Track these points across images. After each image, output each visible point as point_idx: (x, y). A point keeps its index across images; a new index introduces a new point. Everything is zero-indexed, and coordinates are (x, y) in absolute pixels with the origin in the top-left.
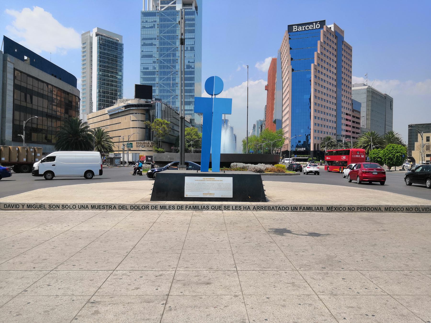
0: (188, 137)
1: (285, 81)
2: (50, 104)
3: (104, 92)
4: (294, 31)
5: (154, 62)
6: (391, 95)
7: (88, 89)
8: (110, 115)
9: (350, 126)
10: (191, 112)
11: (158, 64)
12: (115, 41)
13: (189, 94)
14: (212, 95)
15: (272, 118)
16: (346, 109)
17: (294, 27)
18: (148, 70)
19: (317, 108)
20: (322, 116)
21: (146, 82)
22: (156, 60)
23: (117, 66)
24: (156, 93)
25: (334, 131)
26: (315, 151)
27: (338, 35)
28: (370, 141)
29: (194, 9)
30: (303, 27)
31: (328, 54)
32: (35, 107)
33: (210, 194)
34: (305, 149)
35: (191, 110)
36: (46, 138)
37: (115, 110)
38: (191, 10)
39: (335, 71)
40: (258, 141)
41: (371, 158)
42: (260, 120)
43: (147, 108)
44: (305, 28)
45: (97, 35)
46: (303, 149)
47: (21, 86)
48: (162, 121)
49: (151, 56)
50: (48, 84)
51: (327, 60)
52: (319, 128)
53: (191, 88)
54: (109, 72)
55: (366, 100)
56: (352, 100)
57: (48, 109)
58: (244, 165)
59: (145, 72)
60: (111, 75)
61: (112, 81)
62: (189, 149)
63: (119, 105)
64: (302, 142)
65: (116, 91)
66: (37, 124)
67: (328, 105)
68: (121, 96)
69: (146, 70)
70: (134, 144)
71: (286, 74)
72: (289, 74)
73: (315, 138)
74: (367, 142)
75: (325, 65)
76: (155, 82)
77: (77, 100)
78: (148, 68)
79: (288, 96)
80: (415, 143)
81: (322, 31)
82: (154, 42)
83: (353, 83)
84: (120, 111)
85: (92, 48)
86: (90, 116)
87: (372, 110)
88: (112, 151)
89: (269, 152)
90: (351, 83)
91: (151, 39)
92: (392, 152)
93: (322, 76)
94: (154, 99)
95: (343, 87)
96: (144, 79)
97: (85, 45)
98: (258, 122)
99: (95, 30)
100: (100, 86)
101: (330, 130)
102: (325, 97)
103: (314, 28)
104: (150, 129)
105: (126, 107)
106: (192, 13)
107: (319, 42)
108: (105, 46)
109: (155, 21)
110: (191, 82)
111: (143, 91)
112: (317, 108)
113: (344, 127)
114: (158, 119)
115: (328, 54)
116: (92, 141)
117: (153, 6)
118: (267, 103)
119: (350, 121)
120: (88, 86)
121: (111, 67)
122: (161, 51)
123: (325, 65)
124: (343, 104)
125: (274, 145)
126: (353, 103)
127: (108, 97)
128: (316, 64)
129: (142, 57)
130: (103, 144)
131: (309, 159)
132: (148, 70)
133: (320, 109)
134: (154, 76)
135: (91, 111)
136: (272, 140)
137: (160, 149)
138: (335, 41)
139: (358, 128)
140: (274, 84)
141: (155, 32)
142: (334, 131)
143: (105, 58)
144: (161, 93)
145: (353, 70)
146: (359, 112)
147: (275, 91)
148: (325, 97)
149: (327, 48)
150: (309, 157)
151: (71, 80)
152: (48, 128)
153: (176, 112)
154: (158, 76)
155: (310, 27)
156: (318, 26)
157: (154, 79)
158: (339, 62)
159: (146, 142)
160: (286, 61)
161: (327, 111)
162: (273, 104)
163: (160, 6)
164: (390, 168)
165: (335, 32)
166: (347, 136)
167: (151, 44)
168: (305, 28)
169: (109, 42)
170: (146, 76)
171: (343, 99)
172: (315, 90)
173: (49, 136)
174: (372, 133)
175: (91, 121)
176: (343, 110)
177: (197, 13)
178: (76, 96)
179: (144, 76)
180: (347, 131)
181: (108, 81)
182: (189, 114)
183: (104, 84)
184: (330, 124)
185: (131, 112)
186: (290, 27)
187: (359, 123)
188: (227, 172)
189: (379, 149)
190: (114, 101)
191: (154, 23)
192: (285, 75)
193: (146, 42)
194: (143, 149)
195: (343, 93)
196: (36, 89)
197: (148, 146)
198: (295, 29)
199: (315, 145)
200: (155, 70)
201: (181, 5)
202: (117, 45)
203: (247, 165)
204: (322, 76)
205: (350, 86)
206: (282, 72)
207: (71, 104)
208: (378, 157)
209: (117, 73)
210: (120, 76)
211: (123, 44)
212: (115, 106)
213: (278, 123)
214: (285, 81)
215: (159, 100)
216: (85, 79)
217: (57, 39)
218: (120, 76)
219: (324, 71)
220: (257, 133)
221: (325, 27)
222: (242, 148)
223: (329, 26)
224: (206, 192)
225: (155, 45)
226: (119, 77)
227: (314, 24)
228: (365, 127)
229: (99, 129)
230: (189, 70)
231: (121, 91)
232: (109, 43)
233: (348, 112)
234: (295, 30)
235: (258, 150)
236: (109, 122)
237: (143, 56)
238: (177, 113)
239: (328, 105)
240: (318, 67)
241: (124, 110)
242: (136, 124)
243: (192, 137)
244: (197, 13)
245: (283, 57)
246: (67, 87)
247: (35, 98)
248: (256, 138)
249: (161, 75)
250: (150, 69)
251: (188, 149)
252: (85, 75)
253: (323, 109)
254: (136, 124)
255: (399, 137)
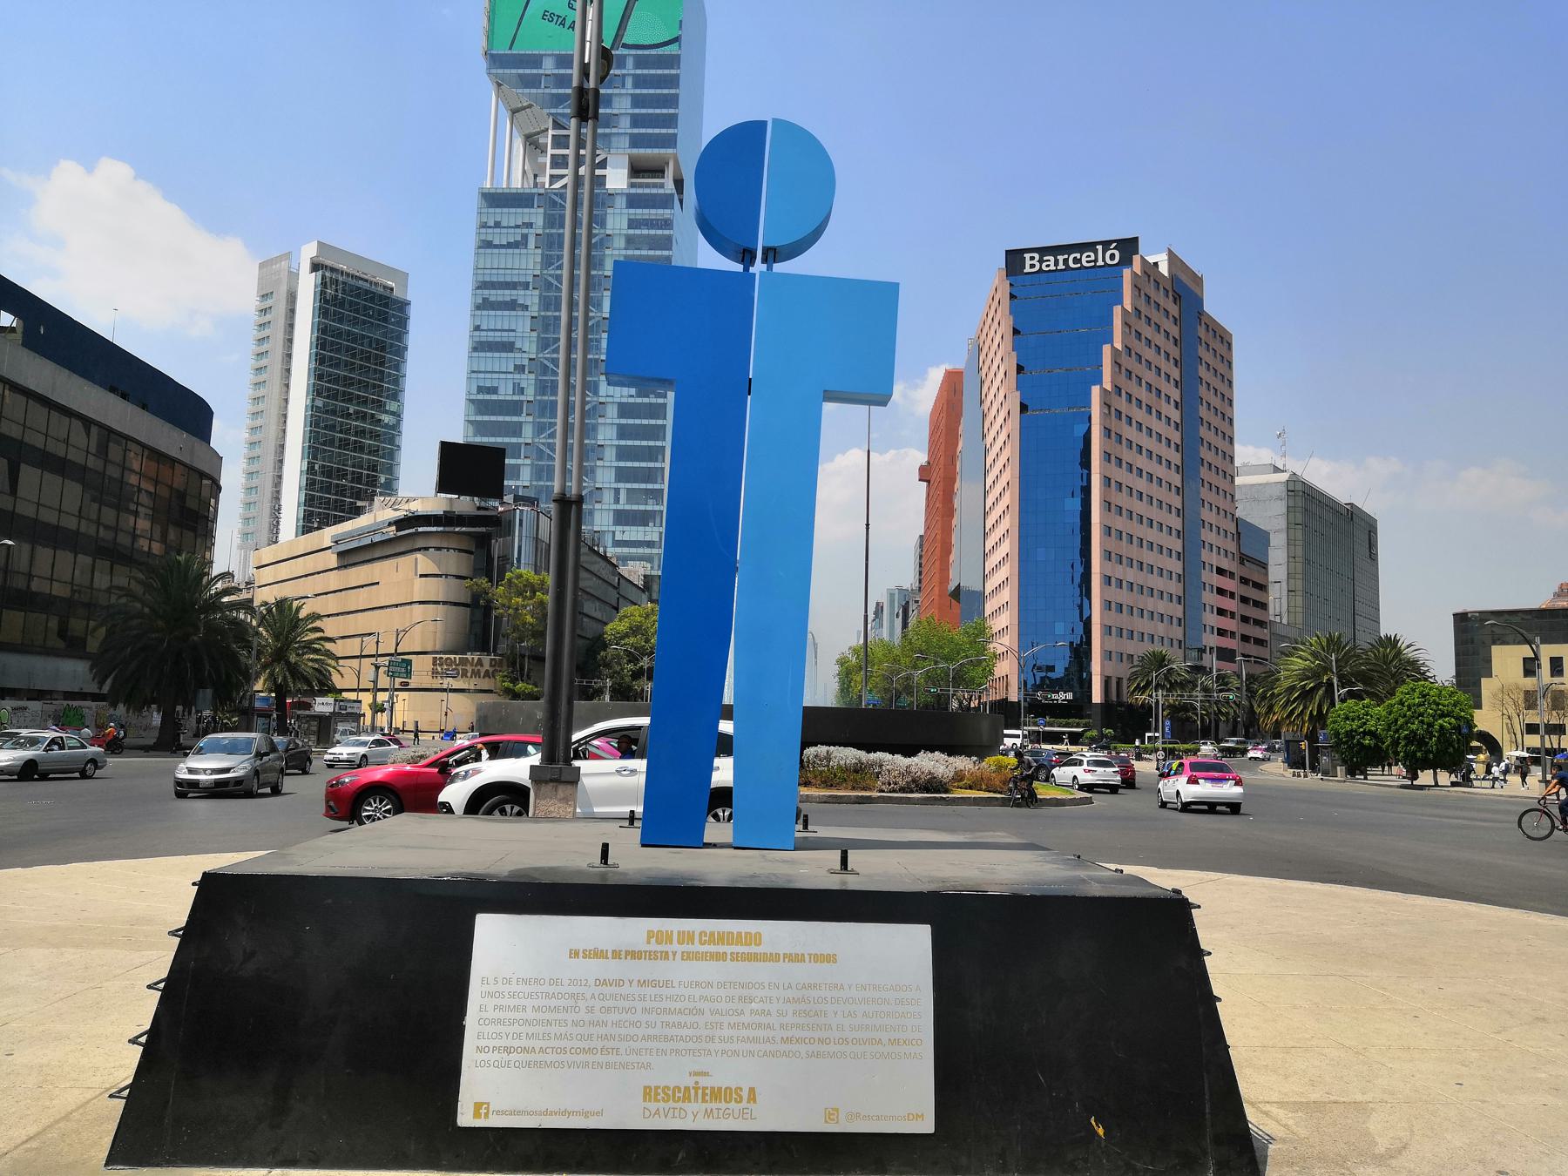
0: (632, 640)
1: (996, 449)
2: (94, 500)
3: (327, 472)
4: (1027, 269)
5: (520, 369)
6: (1368, 507)
7: (270, 459)
8: (341, 554)
9: (1233, 615)
10: (647, 551)
11: (532, 376)
12: (380, 290)
13: (643, 486)
14: (747, 256)
15: (945, 579)
16: (1216, 552)
17: (1027, 256)
18: (494, 397)
19: (1113, 545)
20: (1131, 575)
21: (485, 440)
22: (526, 362)
23: (382, 380)
24: (521, 476)
25: (1178, 633)
26: (1107, 705)
27: (1181, 292)
28: (1327, 669)
29: (669, 186)
30: (1061, 258)
31: (1149, 354)
32: (27, 510)
33: (716, 1094)
34: (1070, 696)
35: (650, 544)
36: (62, 633)
37: (360, 534)
38: (661, 191)
39: (1175, 416)
40: (896, 660)
41: (1337, 734)
42: (900, 590)
43: (483, 529)
44: (1065, 261)
45: (315, 267)
46: (1063, 697)
47: (21, 442)
48: (534, 579)
49: (508, 347)
50: (87, 422)
51: (1149, 376)
52: (1124, 620)
53: (651, 465)
54: (350, 401)
55: (1282, 523)
56: (1237, 521)
57: (80, 517)
58: (862, 755)
59: (484, 403)
60: (357, 412)
61: (361, 433)
62: (636, 686)
63: (379, 515)
64: (1059, 672)
65: (373, 467)
66: (30, 576)
67: (1152, 535)
68: (390, 488)
69: (487, 397)
70: (422, 666)
71: (1000, 420)
72: (1009, 422)
73: (1107, 655)
74: (1315, 674)
75: (1142, 393)
76: (521, 440)
77: (205, 493)
78: (494, 390)
79: (1006, 500)
80: (1483, 680)
81: (1127, 273)
82: (520, 295)
83: (1237, 463)
84: (377, 538)
85: (292, 311)
86: (268, 554)
87: (1307, 561)
88: (327, 688)
89: (942, 701)
90: (1232, 458)
91: (512, 286)
92: (1421, 715)
93: (1130, 433)
94: (508, 498)
95: (1204, 472)
96: (479, 427)
97: (269, 303)
98: (892, 595)
99: (309, 252)
100: (315, 448)
101: (1160, 629)
102: (1140, 507)
103: (1100, 263)
104: (488, 608)
105: (400, 524)
106: (665, 201)
107: (1117, 310)
108: (342, 305)
109: (530, 225)
110: (651, 443)
111: (467, 467)
112: (1113, 545)
113: (1212, 619)
114: (522, 570)
115: (1149, 354)
116: (248, 647)
117: (524, 172)
118: (927, 528)
119: (1232, 595)
120: (271, 446)
121: (360, 382)
122: (546, 330)
123: (1142, 393)
124: (1209, 536)
125: (959, 679)
126: (1242, 530)
127: (341, 491)
128: (1108, 386)
129: (475, 349)
130: (293, 658)
131: (1089, 734)
132: (494, 397)
133: (1124, 548)
134: (515, 419)
135: (274, 540)
136: (947, 659)
137: (521, 686)
138: (1174, 310)
139: (1260, 623)
140: (951, 458)
141: (528, 262)
142: (1178, 633)
143: (338, 351)
144: (540, 479)
145: (1239, 412)
146: (1264, 566)
147: (957, 485)
148: (1140, 507)
149: (1148, 332)
150: (1085, 725)
151: (193, 414)
152: (73, 592)
153: (591, 549)
154: (530, 419)
155: (1086, 258)
156: (1112, 257)
157: (516, 430)
158: (1188, 384)
159: (469, 656)
160: (1001, 375)
161: (1149, 557)
162: (947, 530)
163: (549, 171)
164: (1415, 777)
165: (1173, 277)
166: (1225, 655)
167: (512, 305)
168: (1065, 261)
169: (358, 292)
170: (486, 418)
171: (1208, 515)
172: (1107, 481)
173: (77, 626)
174: (1330, 640)
175: (267, 575)
176: (1205, 555)
177: (681, 201)
178: (203, 475)
179: (479, 418)
180: (1221, 632)
181: (347, 431)
182: (641, 558)
183: (331, 443)
184: (1162, 606)
185: (420, 543)
186: (1014, 259)
187: (1263, 606)
188: (876, 870)
189: (1367, 701)
190: (359, 504)
191: (525, 231)
192: (996, 427)
193: (492, 295)
194: (456, 684)
195: (1204, 493)
196: (37, 441)
197: (476, 674)
198: (1031, 263)
199: (1107, 682)
200: (523, 398)
201: (626, 171)
202: (386, 305)
203: (873, 756)
204: (1130, 433)
205: (1229, 471)
206: (984, 416)
207: (189, 506)
208: (1365, 733)
209: (380, 406)
210: (393, 413)
211: (409, 303)
212: (363, 521)
213: (966, 601)
214: (996, 449)
215: (530, 501)
216: (259, 422)
217: (172, 281)
218: (393, 413)
219: (1139, 415)
220: (889, 632)
221: (1136, 259)
222: (834, 685)
223: (1151, 259)
224: (675, 1073)
225: (525, 308)
226: (386, 418)
227: (1099, 248)
228: (1285, 621)
229: (281, 604)
230: (646, 400)
231: (390, 470)
232: (358, 296)
233: (1225, 564)
234: (1032, 266)
235: (898, 697)
236: (334, 580)
237: (479, 347)
238: (597, 553)
239: (1152, 535)
240: (1114, 397)
241: (391, 535)
242: (435, 589)
243: (647, 641)
244: (681, 201)
245: (988, 362)
246: (169, 439)
247: (29, 474)
248: (888, 648)
249: (542, 415)
250: (501, 391)
251: (630, 688)
252: (261, 406)
253: (1133, 552)
254: (435, 589)
255: (1422, 656)
